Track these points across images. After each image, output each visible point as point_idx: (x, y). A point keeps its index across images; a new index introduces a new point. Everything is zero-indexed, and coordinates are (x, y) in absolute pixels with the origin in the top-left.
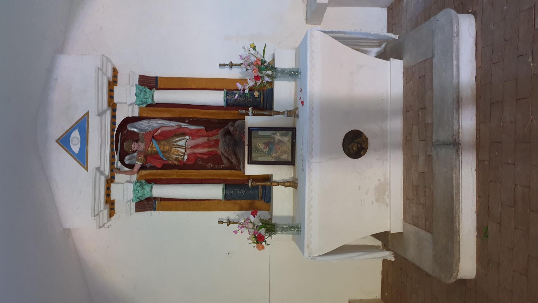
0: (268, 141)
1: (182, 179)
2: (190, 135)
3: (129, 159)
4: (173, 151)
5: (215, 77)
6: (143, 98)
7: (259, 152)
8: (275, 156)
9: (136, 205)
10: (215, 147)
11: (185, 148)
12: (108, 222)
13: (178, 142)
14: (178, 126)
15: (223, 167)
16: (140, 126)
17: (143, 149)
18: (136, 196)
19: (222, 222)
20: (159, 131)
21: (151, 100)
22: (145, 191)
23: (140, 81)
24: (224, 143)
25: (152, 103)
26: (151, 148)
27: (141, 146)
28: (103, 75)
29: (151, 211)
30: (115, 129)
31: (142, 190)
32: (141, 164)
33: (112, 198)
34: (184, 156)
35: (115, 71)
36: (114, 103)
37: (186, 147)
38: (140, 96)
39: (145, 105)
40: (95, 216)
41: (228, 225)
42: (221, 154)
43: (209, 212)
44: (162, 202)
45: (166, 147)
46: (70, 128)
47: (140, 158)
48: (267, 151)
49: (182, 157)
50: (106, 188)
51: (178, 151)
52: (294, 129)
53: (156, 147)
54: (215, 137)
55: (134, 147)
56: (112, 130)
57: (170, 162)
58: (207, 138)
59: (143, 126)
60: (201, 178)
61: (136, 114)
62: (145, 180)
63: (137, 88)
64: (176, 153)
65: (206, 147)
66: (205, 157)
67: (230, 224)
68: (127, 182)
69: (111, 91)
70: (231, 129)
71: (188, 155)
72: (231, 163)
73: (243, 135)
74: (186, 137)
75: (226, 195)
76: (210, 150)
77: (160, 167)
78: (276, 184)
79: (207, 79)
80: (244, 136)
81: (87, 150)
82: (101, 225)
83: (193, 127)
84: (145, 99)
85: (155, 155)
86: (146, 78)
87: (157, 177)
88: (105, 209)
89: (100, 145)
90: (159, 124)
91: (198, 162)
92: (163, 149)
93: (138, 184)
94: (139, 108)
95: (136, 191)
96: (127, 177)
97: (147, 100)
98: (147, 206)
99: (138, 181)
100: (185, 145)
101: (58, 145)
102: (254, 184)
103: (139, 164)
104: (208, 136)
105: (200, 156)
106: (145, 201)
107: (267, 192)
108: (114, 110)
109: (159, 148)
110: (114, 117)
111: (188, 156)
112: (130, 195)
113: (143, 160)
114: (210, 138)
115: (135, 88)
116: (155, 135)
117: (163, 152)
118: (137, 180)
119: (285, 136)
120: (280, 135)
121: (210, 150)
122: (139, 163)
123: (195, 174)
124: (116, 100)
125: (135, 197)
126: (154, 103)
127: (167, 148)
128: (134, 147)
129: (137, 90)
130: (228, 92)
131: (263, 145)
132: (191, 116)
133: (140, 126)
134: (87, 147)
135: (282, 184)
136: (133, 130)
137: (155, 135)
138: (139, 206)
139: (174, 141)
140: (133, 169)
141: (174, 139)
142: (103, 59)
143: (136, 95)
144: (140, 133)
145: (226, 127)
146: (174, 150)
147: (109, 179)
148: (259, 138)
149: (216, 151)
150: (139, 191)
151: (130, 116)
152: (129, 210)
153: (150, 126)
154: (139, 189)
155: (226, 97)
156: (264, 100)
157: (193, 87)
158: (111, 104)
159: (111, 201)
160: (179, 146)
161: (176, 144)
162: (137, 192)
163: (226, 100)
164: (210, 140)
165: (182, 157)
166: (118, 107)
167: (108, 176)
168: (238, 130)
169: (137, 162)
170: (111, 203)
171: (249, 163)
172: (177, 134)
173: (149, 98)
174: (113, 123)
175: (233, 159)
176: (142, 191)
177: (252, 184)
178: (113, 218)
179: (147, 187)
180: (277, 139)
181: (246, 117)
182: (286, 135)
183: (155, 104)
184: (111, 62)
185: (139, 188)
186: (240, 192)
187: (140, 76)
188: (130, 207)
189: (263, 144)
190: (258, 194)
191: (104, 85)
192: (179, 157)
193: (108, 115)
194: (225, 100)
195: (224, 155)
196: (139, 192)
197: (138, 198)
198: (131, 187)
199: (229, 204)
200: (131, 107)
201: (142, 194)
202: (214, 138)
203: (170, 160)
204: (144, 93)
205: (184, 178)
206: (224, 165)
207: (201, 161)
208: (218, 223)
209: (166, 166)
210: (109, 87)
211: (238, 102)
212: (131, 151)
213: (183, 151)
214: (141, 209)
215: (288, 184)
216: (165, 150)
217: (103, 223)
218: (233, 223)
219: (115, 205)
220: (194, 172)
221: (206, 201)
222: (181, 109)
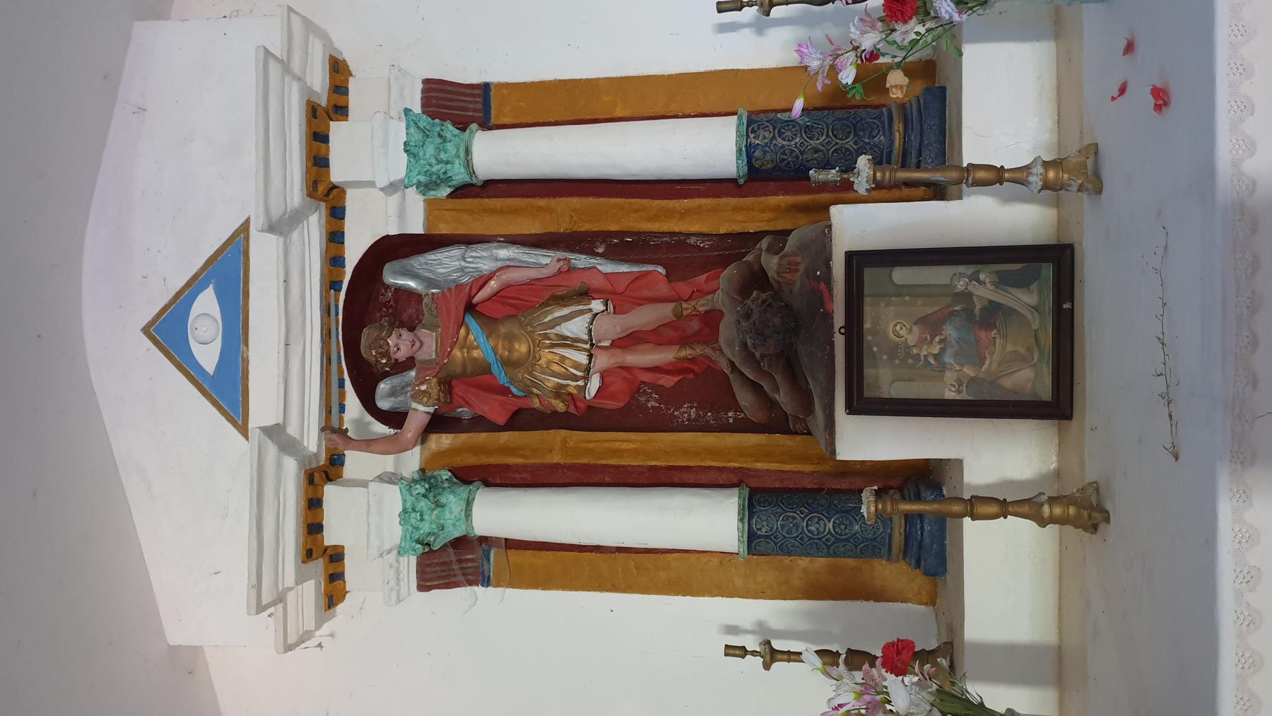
0: (936, 309)
1: (585, 465)
2: (605, 295)
3: (393, 393)
4: (543, 362)
5: (702, 69)
6: (434, 161)
7: (897, 362)
8: (972, 380)
9: (419, 564)
10: (706, 343)
11: (588, 346)
12: (1119, 96)
13: (563, 325)
14: (562, 263)
15: (735, 419)
16: (430, 271)
17: (434, 357)
18: (412, 533)
19: (742, 652)
20: (493, 285)
21: (463, 170)
22: (447, 515)
23: (426, 103)
24: (744, 324)
25: (467, 179)
26: (462, 348)
27: (427, 344)
28: (287, 79)
29: (475, 588)
30: (341, 282)
31: (433, 510)
32: (431, 410)
33: (331, 537)
34: (586, 378)
35: (338, 70)
36: (334, 187)
37: (592, 345)
38: (421, 154)
39: (444, 192)
40: (260, 609)
41: (767, 666)
42: (727, 371)
43: (689, 598)
44: (514, 556)
45: (517, 347)
46: (188, 284)
47: (423, 388)
48: (936, 357)
49: (581, 383)
50: (303, 503)
51: (563, 358)
52: (1068, 252)
53: (482, 346)
54: (702, 301)
55: (397, 345)
56: (331, 285)
57: (536, 403)
58: (670, 306)
59: (442, 271)
60: (653, 463)
61: (416, 226)
62: (449, 471)
63: (412, 123)
64: (556, 368)
65: (670, 343)
66: (668, 381)
67: (773, 660)
68: (383, 478)
69: (317, 138)
70: (771, 264)
71: (604, 375)
72: (771, 404)
73: (822, 286)
74: (591, 306)
75: (753, 540)
76: (686, 353)
77: (501, 420)
78: (994, 509)
79: (670, 77)
80: (830, 289)
81: (246, 361)
82: (291, 641)
83: (624, 268)
84: (440, 166)
85: (479, 376)
86: (449, 88)
87: (493, 460)
88: (300, 580)
89: (282, 344)
90: (503, 260)
91: (643, 399)
92: (507, 353)
93: (420, 489)
94: (424, 200)
95: (413, 515)
96: (386, 463)
97: (449, 166)
98: (455, 567)
99: (424, 474)
100: (586, 337)
101: (148, 343)
102: (889, 508)
103: (420, 412)
104: (677, 299)
105: (646, 377)
106: (451, 550)
107: (927, 528)
108: (337, 213)
109: (490, 351)
110: (335, 237)
111: (602, 378)
112: (394, 532)
113: (434, 395)
114: (685, 305)
115: (404, 124)
116: (477, 299)
117: (507, 363)
118: (422, 470)
119: (1019, 286)
120: (993, 283)
121: (686, 353)
122: (421, 408)
123: (632, 446)
124: (337, 175)
125: (408, 537)
126: (474, 181)
127: (522, 348)
128: (397, 345)
129: (412, 130)
130: (753, 117)
131: (916, 329)
132: (613, 228)
133: (430, 271)
134: (245, 348)
135: (1026, 509)
136: (402, 285)
137: (477, 299)
138: (428, 569)
139: (546, 320)
140: (401, 428)
141: (551, 312)
142: (289, 24)
143: (406, 151)
144: (425, 296)
145: (749, 258)
146: (550, 357)
147: (318, 469)
148: (907, 298)
149: (708, 358)
150: (421, 515)
151: (393, 231)
152: (393, 583)
153: (466, 270)
154: (425, 509)
155: (748, 136)
156: (905, 143)
157: (619, 114)
158: (322, 188)
159: (326, 548)
160: (566, 338)
161: (553, 331)
162: (415, 517)
163: (748, 152)
164: (685, 313)
165: (581, 383)
166: (353, 202)
167: (316, 455)
168: (802, 268)
169: (414, 405)
170: (331, 556)
171: (852, 409)
172: (560, 292)
173: (457, 161)
174: (334, 260)
175: (777, 390)
176: (435, 512)
177: (880, 506)
178: (340, 608)
179: (451, 497)
180: (980, 298)
181: (836, 211)
182: (1022, 282)
183: (480, 184)
184: (324, 36)
185: (423, 504)
186: (812, 528)
187: (428, 83)
188: (398, 572)
189: (915, 323)
190: (890, 536)
191: (290, 115)
192: (570, 382)
193: (314, 226)
194: (744, 149)
195: (742, 374)
196: (422, 520)
197: (418, 542)
198: (393, 498)
199: (767, 569)
200: (395, 199)
201: (434, 526)
202: (702, 305)
203: (537, 395)
204: (439, 140)
205: (592, 462)
206: (742, 411)
207: (654, 395)
208: (726, 655)
209: (522, 419)
210: (309, 123)
211: (797, 157)
212: (384, 361)
213: (582, 358)
214: (439, 578)
215: (1058, 511)
216: (515, 356)
217: (301, 633)
218: (785, 657)
219: (346, 560)
220: (631, 441)
221: (675, 555)
222: (575, 202)
